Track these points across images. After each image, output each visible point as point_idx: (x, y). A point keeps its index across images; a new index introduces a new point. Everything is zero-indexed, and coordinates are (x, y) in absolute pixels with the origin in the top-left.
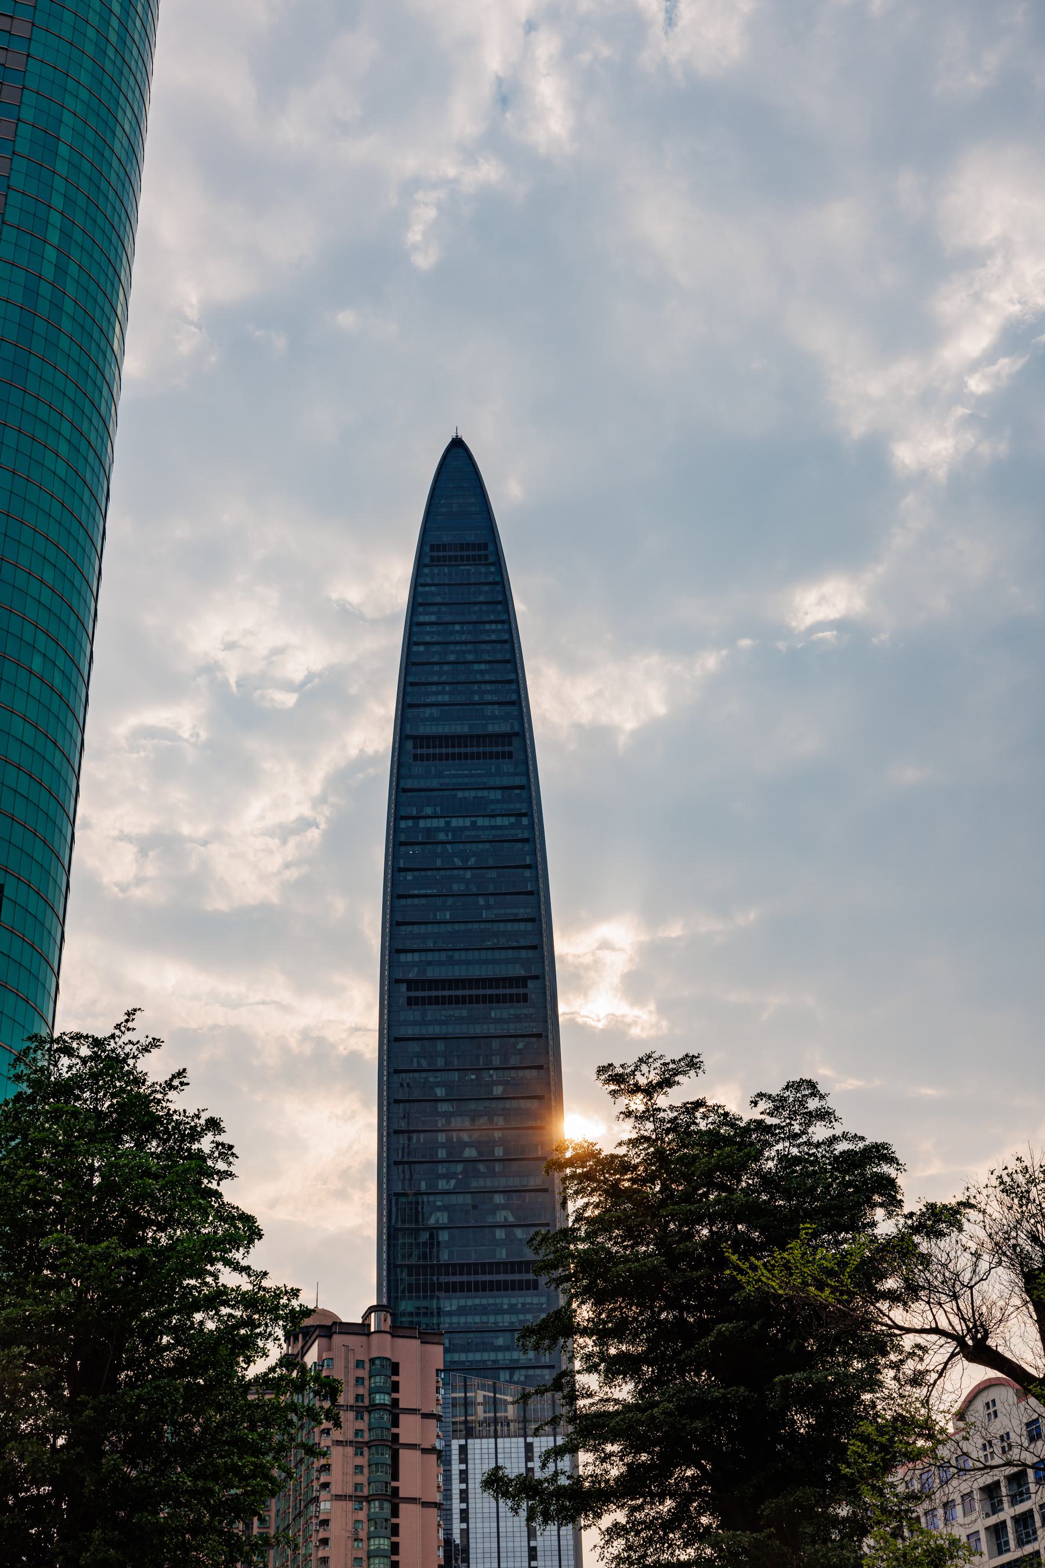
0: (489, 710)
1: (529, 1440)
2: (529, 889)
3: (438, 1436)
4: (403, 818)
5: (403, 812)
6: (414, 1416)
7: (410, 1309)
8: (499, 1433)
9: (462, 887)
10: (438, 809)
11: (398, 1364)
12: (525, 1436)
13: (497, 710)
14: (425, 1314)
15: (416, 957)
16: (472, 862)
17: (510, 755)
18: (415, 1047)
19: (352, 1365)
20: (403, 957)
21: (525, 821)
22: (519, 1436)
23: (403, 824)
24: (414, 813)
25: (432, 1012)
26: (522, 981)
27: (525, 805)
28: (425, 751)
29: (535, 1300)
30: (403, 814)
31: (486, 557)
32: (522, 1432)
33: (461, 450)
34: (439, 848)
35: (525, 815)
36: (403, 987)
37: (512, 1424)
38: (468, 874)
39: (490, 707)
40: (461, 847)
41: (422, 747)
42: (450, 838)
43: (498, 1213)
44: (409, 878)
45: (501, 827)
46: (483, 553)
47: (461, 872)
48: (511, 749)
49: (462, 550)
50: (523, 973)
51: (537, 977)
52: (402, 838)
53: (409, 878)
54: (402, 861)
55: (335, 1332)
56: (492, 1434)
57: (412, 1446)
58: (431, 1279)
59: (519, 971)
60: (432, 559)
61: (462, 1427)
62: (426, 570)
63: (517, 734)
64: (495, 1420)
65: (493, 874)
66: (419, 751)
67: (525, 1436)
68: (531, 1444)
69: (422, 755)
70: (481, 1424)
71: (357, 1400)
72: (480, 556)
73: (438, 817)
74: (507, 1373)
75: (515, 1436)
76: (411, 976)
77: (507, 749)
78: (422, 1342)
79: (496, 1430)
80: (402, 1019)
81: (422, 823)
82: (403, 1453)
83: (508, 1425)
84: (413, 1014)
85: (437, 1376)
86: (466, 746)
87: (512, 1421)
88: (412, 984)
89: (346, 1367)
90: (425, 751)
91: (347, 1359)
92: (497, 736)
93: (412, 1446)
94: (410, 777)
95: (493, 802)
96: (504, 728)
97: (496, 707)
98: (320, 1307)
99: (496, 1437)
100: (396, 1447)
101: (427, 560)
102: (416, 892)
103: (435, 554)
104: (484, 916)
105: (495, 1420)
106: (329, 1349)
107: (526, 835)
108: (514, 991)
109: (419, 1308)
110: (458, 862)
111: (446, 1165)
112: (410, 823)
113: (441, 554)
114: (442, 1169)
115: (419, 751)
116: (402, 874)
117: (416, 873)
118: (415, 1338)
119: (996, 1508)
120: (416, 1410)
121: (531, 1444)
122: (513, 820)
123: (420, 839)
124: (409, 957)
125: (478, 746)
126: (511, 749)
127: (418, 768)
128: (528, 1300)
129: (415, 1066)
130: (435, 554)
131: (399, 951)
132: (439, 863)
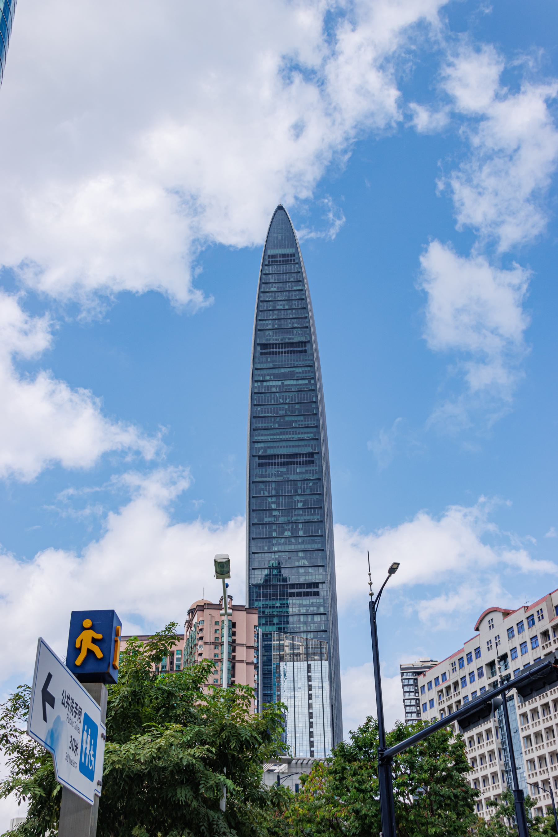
0: (295, 331)
1: (309, 663)
2: (315, 412)
3: (255, 657)
4: (256, 381)
5: (256, 379)
6: (243, 647)
7: (260, 605)
8: (295, 660)
9: (284, 412)
10: (272, 377)
11: (235, 623)
12: (307, 661)
13: (300, 331)
14: (267, 607)
15: (262, 445)
16: (287, 401)
17: (306, 351)
18: (262, 486)
19: (213, 623)
20: (256, 445)
21: (312, 381)
22: (304, 661)
23: (256, 384)
24: (261, 379)
25: (271, 470)
26: (311, 455)
27: (313, 374)
28: (266, 351)
29: (318, 601)
30: (256, 380)
31: (294, 260)
32: (306, 659)
33: (282, 211)
34: (273, 395)
35: (313, 378)
36: (257, 458)
37: (301, 655)
38: (286, 407)
39: (296, 329)
40: (283, 394)
41: (264, 349)
42: (278, 390)
43: (300, 561)
44: (259, 409)
45: (301, 385)
46: (292, 258)
47: (283, 406)
48: (306, 348)
49: (283, 257)
50: (312, 451)
51: (318, 453)
52: (256, 391)
53: (259, 409)
54: (255, 402)
55: (205, 608)
56: (292, 660)
57: (242, 661)
58: (270, 592)
59: (310, 450)
60: (269, 262)
61: (278, 657)
62: (266, 267)
63: (309, 342)
64: (293, 654)
65: (297, 406)
66: (263, 351)
67: (307, 661)
68: (310, 665)
69: (265, 352)
70: (286, 655)
71: (215, 640)
72: (291, 260)
73: (272, 381)
74: (305, 634)
75: (303, 661)
76: (260, 453)
77: (304, 348)
78: (247, 613)
79: (293, 658)
80: (255, 473)
81: (265, 384)
82: (238, 665)
83: (299, 656)
84: (259, 471)
85: (255, 629)
86: (285, 348)
87: (301, 654)
88: (260, 457)
89: (211, 625)
90: (266, 351)
91: (211, 620)
92: (299, 343)
93: (242, 661)
94: (259, 363)
95: (297, 373)
96: (303, 339)
97: (299, 329)
98: (205, 599)
99: (294, 661)
100: (234, 661)
101: (267, 263)
102: (262, 415)
103: (270, 260)
104: (294, 425)
105: (293, 654)
106: (203, 616)
107: (313, 388)
108: (308, 459)
109: (264, 605)
110: (281, 401)
111: (276, 539)
112: (259, 384)
113: (273, 259)
114: (274, 541)
115: (263, 351)
116: (256, 407)
117: (262, 407)
118: (244, 611)
119: (493, 674)
120: (244, 644)
121: (310, 665)
122: (307, 381)
123: (263, 391)
124: (259, 445)
125: (291, 348)
126: (306, 348)
127: (263, 359)
128: (315, 601)
129: (262, 494)
130: (270, 260)
131: (254, 442)
132: (273, 402)
